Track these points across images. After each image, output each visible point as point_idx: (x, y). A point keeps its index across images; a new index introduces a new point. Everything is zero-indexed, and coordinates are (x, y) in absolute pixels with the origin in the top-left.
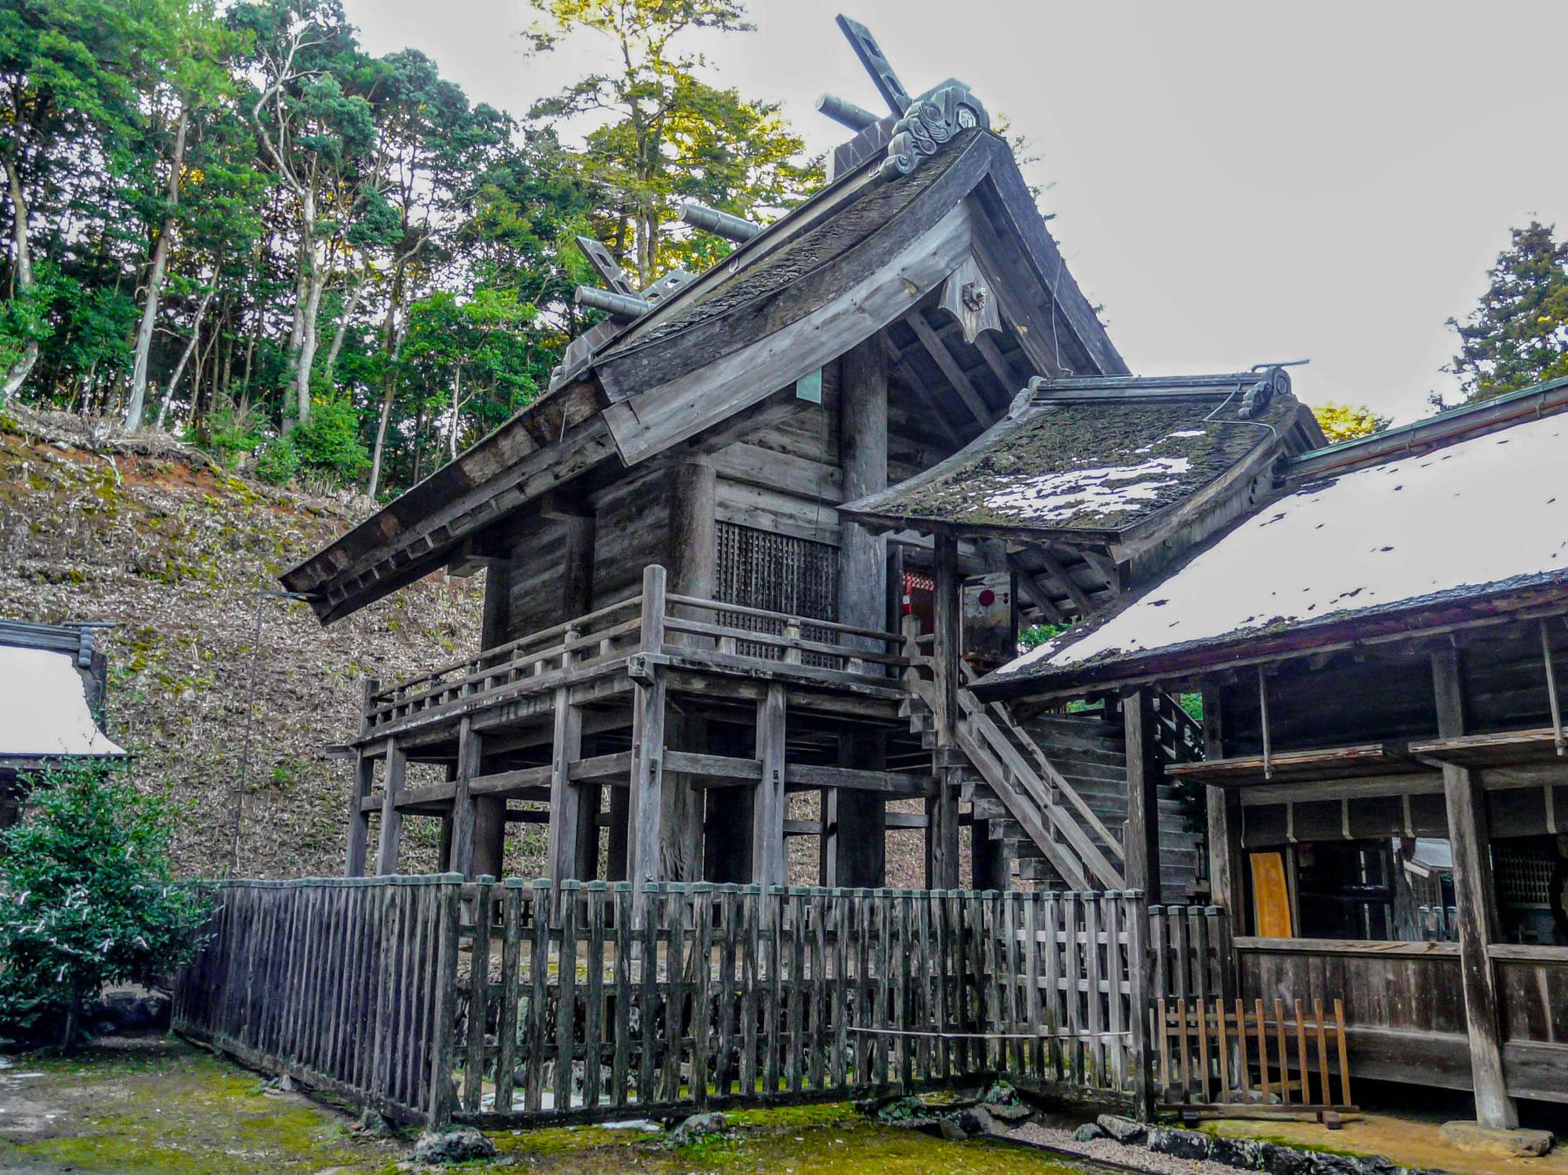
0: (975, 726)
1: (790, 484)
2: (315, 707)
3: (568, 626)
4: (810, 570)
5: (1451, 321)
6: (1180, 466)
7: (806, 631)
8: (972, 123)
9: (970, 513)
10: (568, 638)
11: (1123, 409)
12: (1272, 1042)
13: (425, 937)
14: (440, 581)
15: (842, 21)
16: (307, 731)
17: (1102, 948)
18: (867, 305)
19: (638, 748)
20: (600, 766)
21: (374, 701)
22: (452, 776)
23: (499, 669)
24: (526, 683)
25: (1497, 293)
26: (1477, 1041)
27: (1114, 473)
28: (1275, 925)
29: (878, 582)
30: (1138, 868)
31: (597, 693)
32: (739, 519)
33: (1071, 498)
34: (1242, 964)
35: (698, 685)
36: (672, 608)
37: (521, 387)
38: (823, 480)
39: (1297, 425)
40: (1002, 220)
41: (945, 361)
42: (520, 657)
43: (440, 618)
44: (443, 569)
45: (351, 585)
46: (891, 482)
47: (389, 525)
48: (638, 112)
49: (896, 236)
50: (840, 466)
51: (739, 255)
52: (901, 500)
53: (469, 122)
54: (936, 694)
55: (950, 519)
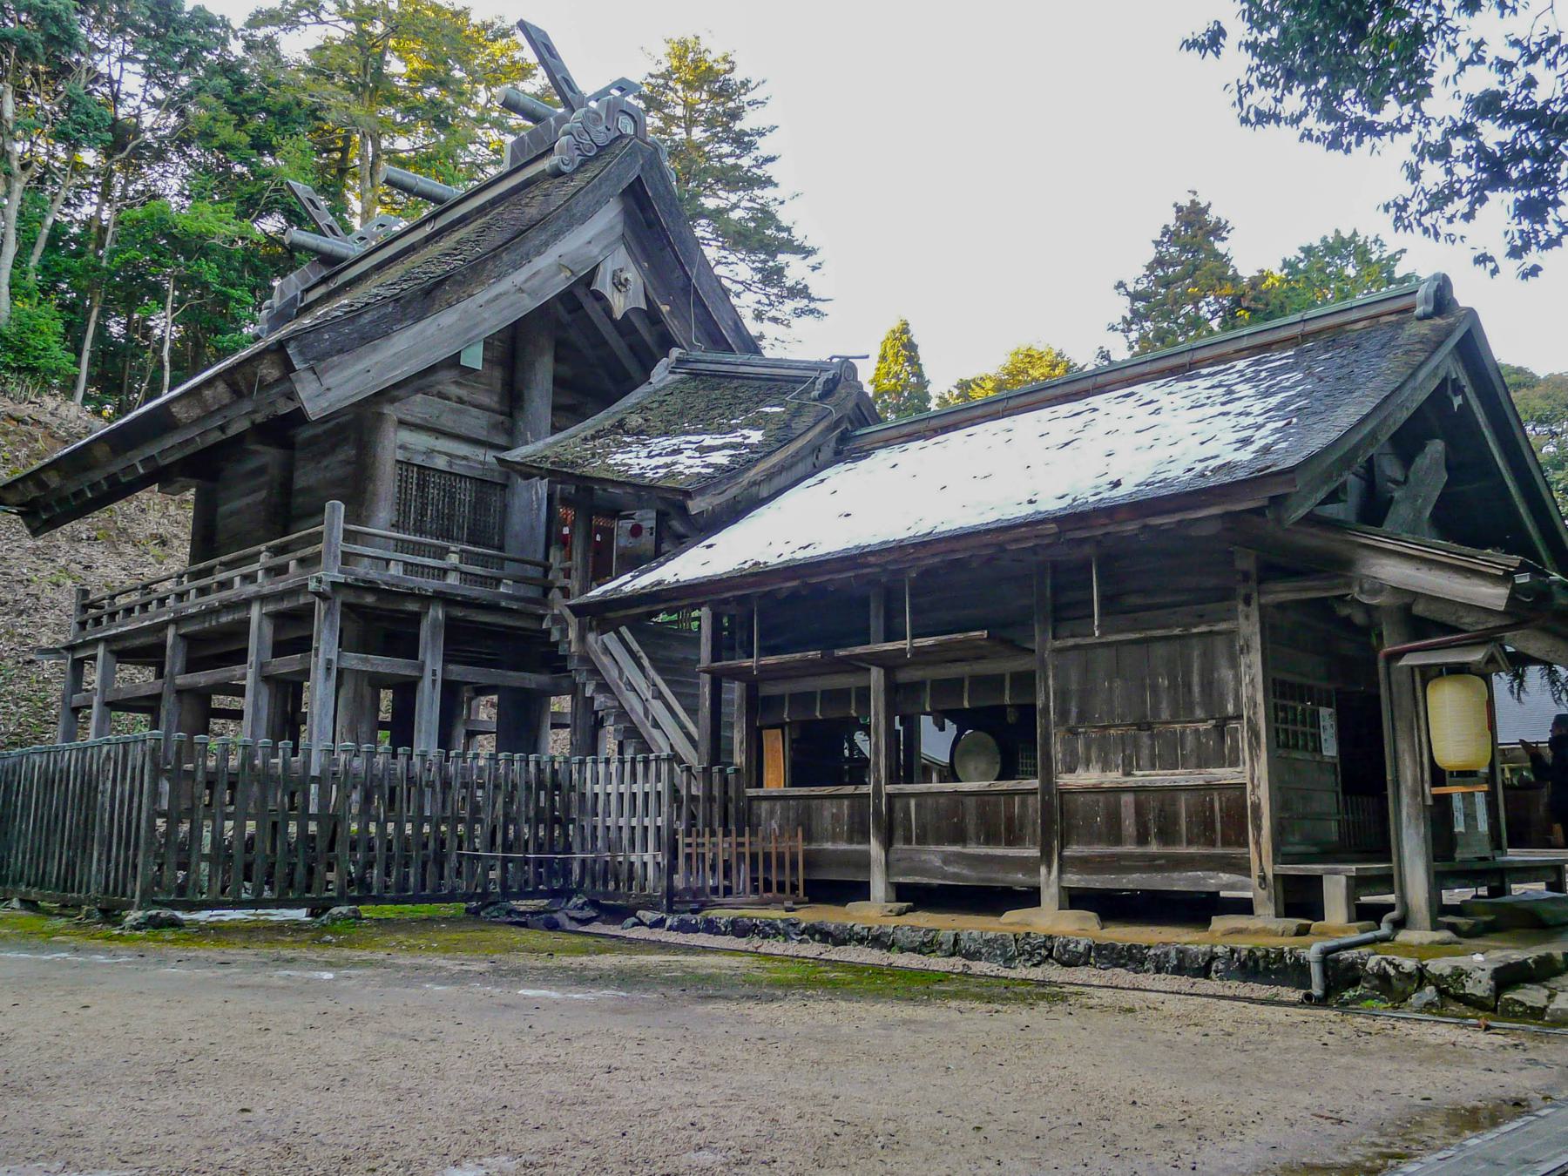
1: (463, 431)
2: (21, 613)
3: (263, 547)
4: (479, 505)
5: (1121, 285)
6: (756, 437)
7: (466, 557)
8: (630, 130)
9: (594, 468)
10: (263, 558)
11: (736, 383)
12: (767, 856)
13: (133, 779)
14: (150, 496)
16: (13, 636)
17: (646, 794)
18: (525, 287)
19: (317, 649)
20: (286, 665)
21: (84, 608)
22: (160, 675)
23: (203, 582)
24: (226, 594)
25: (1159, 262)
26: (875, 848)
27: (708, 440)
28: (775, 781)
29: (538, 515)
30: (705, 747)
31: (285, 605)
32: (418, 460)
33: (669, 460)
34: (750, 808)
35: (370, 599)
36: (349, 536)
37: (238, 301)
38: (495, 427)
39: (857, 405)
43: (151, 528)
44: (156, 487)
45: (62, 501)
46: (555, 429)
47: (102, 452)
48: (362, 33)
49: (552, 229)
50: (511, 415)
51: (433, 217)
52: (547, 453)
53: (182, 27)
55: (578, 472)
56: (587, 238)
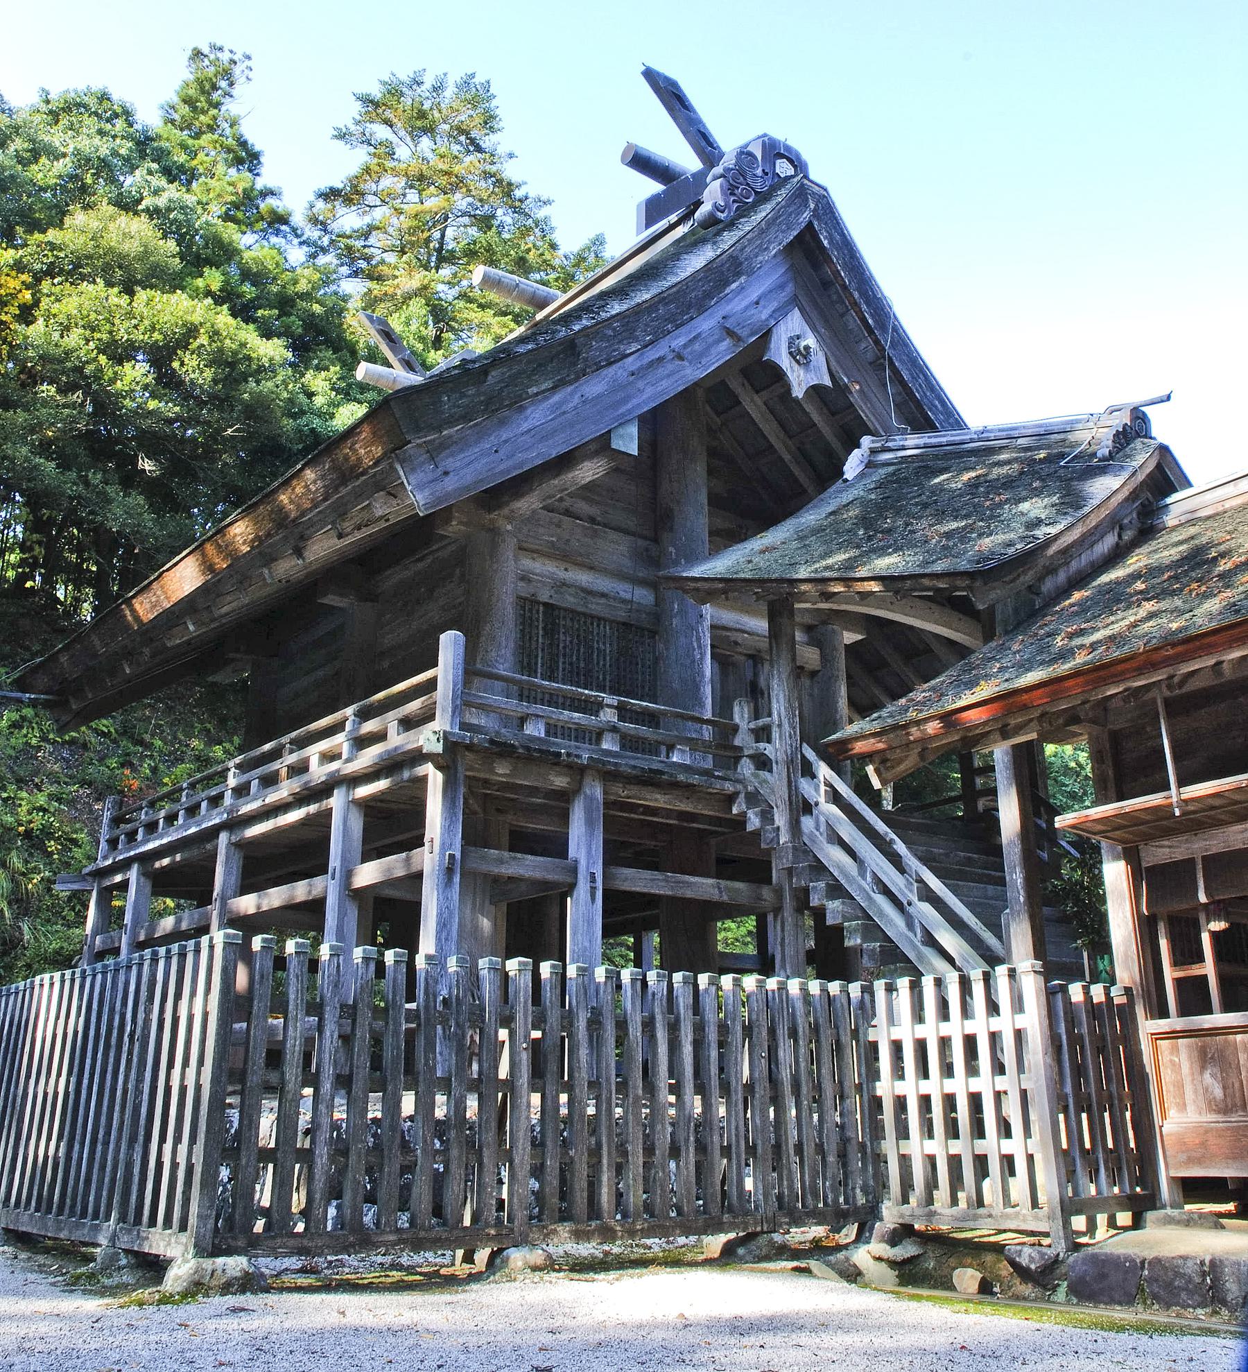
0: (822, 819)
7: (621, 710)
15: (650, 75)
32: (544, 596)
40: (823, 267)
41: (769, 428)
42: (291, 752)
54: (775, 784)
56: (754, 297)
